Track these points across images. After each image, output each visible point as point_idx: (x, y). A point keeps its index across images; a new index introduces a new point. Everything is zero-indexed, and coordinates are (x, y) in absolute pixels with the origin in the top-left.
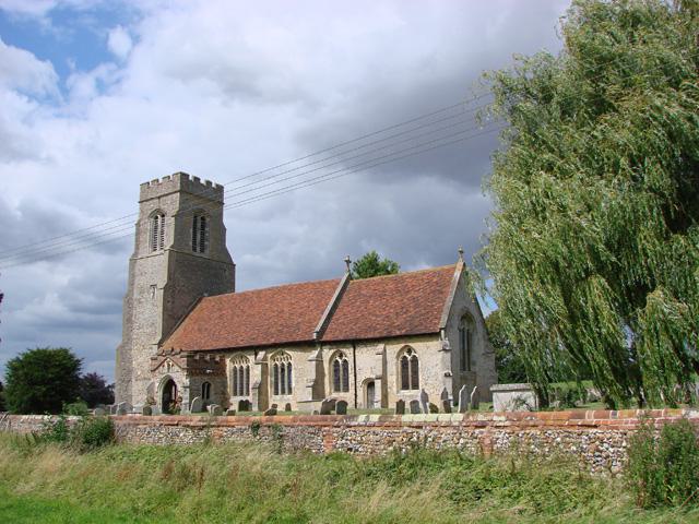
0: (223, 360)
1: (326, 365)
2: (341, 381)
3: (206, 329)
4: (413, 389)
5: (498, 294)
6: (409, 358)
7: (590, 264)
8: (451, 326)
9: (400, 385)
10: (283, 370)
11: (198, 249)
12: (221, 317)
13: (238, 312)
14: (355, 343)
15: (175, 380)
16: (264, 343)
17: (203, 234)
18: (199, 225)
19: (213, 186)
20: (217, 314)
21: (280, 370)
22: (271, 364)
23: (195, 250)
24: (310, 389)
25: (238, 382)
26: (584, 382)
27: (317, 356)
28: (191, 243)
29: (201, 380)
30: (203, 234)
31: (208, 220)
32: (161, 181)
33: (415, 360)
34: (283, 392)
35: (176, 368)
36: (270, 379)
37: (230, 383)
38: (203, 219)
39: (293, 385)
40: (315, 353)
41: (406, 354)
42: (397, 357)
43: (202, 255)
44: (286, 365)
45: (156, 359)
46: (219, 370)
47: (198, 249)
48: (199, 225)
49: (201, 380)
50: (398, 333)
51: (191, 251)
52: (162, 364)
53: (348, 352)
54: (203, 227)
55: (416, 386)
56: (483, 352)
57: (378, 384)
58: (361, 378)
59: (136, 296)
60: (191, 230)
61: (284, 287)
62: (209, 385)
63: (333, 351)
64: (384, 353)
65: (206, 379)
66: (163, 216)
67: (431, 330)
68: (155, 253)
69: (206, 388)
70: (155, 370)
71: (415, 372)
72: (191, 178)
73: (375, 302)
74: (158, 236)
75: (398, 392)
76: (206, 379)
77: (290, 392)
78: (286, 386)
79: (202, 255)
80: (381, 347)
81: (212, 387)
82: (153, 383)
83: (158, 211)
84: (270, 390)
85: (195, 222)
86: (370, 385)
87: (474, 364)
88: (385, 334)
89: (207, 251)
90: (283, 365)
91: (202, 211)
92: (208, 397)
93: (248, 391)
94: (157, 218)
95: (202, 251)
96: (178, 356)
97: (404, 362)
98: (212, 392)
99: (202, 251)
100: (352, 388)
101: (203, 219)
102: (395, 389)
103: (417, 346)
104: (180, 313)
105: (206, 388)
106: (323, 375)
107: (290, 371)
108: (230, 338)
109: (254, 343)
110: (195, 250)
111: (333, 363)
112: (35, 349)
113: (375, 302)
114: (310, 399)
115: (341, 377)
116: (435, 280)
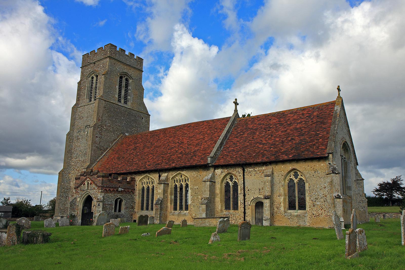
0: (133, 180)
1: (218, 186)
2: (231, 200)
3: (123, 158)
6: (296, 181)
9: (287, 206)
10: (181, 189)
11: (123, 101)
12: (135, 149)
13: (148, 144)
14: (244, 166)
15: (93, 196)
16: (166, 167)
17: (126, 91)
18: (124, 84)
20: (133, 147)
21: (178, 190)
22: (171, 184)
23: (119, 101)
24: (204, 206)
25: (145, 198)
26: (15, 227)
27: (211, 178)
28: (117, 96)
29: (112, 197)
30: (126, 91)
31: (130, 81)
32: (96, 52)
33: (302, 183)
34: (181, 208)
35: (94, 186)
36: (170, 197)
37: (137, 199)
39: (189, 202)
40: (207, 175)
41: (292, 177)
42: (285, 179)
43: (125, 105)
44: (184, 186)
45: (79, 179)
46: (130, 189)
48: (124, 84)
49: (112, 197)
50: (286, 158)
51: (116, 102)
52: (83, 183)
53: (237, 172)
54: (127, 86)
55: (187, 209)
57: (267, 203)
58: (250, 197)
59: (75, 134)
60: (117, 87)
61: (184, 126)
63: (224, 174)
64: (272, 175)
65: (119, 196)
66: (97, 76)
67: (319, 154)
68: (90, 103)
69: (118, 203)
70: (78, 187)
72: (118, 49)
73: (260, 133)
74: (93, 91)
75: (285, 212)
76: (119, 196)
77: (187, 209)
78: (184, 204)
79: (125, 105)
80: (268, 169)
81: (123, 203)
82: (76, 198)
83: (93, 72)
84: (170, 206)
85: (121, 82)
86: (259, 205)
88: (273, 158)
89: (129, 103)
90: (181, 185)
92: (120, 211)
93: (152, 206)
94: (93, 78)
95: (125, 103)
96: (96, 176)
97: (291, 185)
98: (123, 207)
99: (125, 103)
101: (127, 80)
102: (282, 209)
103: (299, 166)
104: (105, 147)
105: (118, 203)
107: (187, 191)
108: (140, 163)
109: (159, 167)
110: (119, 101)
111: (224, 185)
113: (260, 133)
114: (204, 216)
115: (231, 196)
116: (315, 114)
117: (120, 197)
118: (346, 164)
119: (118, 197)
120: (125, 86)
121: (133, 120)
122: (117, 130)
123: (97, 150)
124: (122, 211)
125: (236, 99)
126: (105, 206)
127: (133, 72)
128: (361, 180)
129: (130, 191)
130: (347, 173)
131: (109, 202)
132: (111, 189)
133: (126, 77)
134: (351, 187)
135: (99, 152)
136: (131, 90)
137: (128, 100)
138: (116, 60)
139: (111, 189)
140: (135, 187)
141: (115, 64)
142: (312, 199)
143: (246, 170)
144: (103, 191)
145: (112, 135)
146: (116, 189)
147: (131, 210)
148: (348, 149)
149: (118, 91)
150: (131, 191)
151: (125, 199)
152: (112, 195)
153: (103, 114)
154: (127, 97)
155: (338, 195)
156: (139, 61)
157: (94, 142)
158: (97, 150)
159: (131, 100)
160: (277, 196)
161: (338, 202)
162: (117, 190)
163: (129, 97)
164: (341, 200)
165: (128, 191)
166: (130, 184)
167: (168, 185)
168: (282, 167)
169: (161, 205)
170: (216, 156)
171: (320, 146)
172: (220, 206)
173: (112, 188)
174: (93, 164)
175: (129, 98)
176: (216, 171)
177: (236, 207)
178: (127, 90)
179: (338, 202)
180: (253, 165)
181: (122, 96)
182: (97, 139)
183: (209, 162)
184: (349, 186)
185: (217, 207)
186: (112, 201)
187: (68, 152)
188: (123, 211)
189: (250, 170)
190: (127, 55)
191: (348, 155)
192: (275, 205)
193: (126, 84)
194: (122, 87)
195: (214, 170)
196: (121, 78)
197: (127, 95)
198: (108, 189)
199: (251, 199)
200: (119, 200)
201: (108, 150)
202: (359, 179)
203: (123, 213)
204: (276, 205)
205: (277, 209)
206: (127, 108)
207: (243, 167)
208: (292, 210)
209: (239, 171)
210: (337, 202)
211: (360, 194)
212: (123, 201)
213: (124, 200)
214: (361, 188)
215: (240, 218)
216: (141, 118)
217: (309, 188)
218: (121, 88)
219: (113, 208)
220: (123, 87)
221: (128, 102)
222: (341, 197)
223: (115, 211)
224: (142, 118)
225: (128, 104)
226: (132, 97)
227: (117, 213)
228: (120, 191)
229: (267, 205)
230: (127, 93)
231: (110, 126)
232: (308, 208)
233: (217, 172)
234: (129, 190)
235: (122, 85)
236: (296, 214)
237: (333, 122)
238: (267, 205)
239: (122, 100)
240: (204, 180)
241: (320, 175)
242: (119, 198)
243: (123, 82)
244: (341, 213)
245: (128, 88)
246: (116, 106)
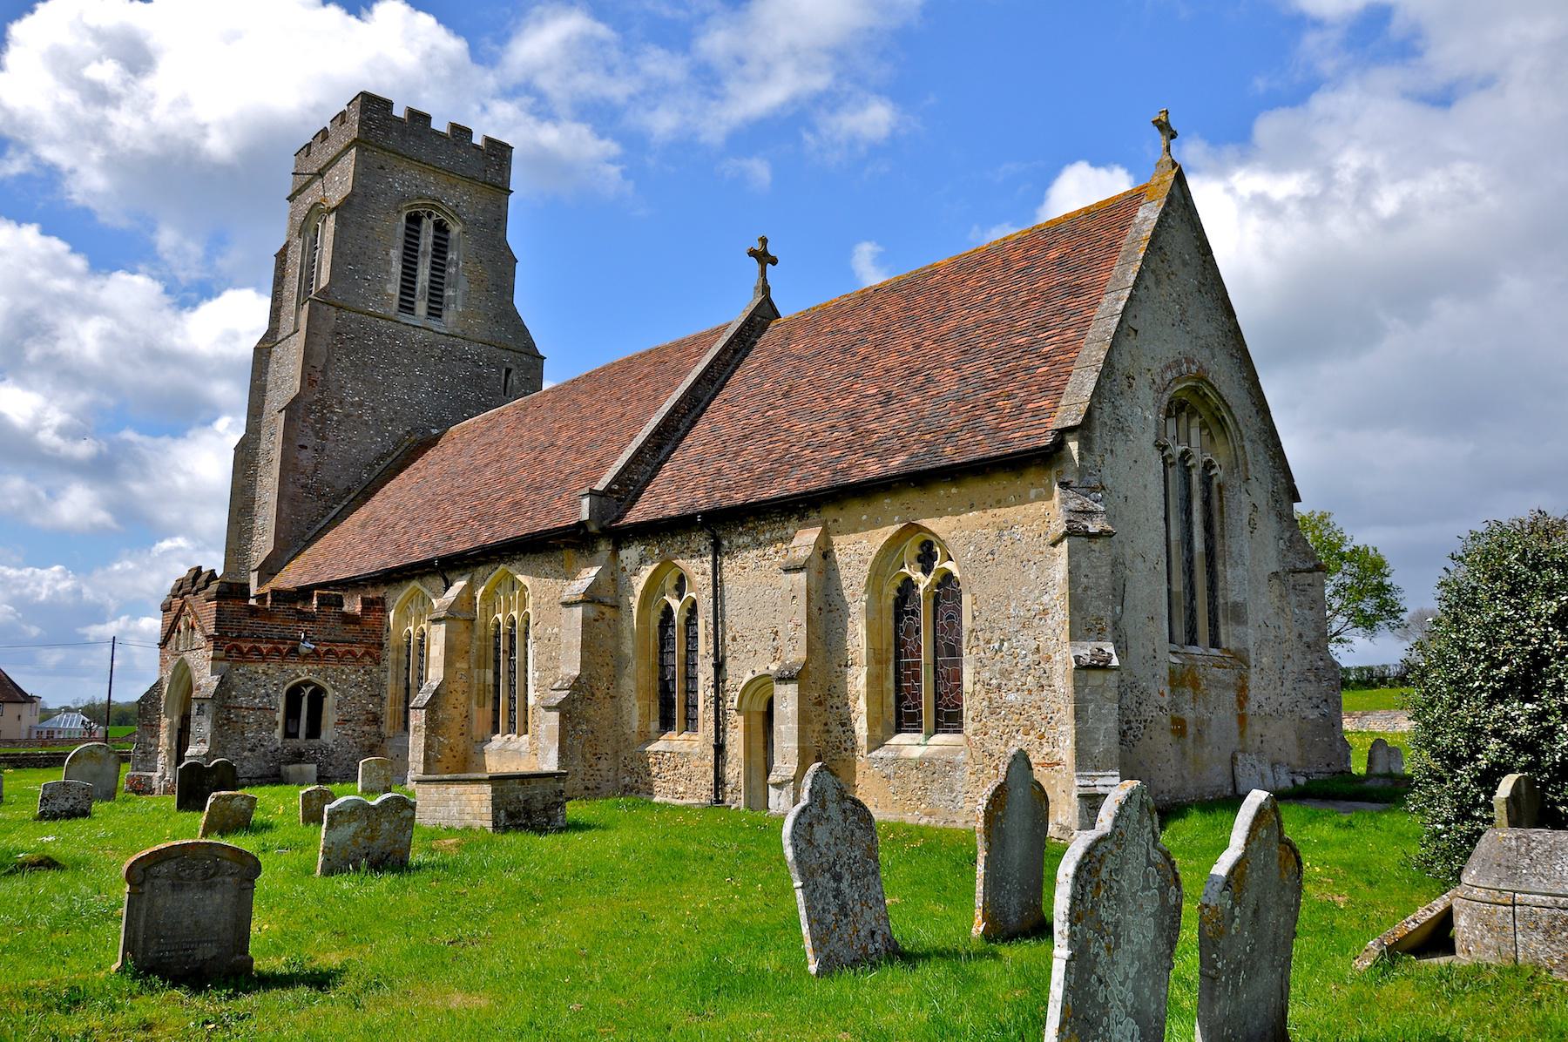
4: (938, 728)
5: (1119, 447)
7: (452, 841)
8: (1120, 427)
11: (421, 307)
17: (438, 268)
19: (477, 140)
23: (407, 306)
28: (394, 289)
30: (438, 268)
31: (455, 229)
38: (440, 227)
43: (433, 324)
47: (421, 307)
50: (874, 469)
54: (440, 249)
56: (1275, 567)
58: (740, 674)
60: (396, 254)
62: (318, 696)
65: (304, 672)
67: (1020, 439)
71: (949, 650)
80: (805, 539)
81: (330, 702)
87: (1238, 614)
89: (450, 316)
91: (435, 204)
92: (314, 730)
95: (435, 312)
98: (330, 716)
99: (435, 312)
100: (705, 713)
101: (440, 227)
106: (618, 665)
110: (407, 306)
112: (1481, 528)
117: (313, 678)
118: (1220, 492)
119: (300, 679)
120: (434, 250)
121: (464, 380)
122: (391, 420)
123: (307, 497)
124: (323, 736)
125: (764, 241)
126: (237, 716)
127: (466, 195)
128: (1309, 571)
129: (359, 651)
130: (1223, 537)
131: (255, 698)
132: (264, 647)
133: (437, 216)
134: (1244, 605)
135: (314, 504)
136: (457, 264)
137: (445, 302)
138: (389, 152)
139: (264, 647)
140: (384, 638)
141: (382, 168)
142: (986, 675)
143: (725, 543)
144: (222, 654)
145: (371, 439)
146: (286, 643)
147: (366, 728)
148: (1223, 417)
149: (397, 268)
150: (367, 653)
151: (334, 688)
152: (270, 672)
153: (328, 360)
154: (442, 290)
155: (1099, 650)
156: (494, 156)
157: (290, 467)
158: (307, 497)
159: (459, 302)
160: (840, 666)
161: (1091, 692)
162: (294, 650)
163: (449, 292)
164: (1113, 678)
165: (349, 652)
166: (359, 624)
167: (470, 627)
168: (864, 517)
169: (434, 712)
170: (627, 486)
171: (1033, 397)
172: (636, 712)
173: (269, 640)
174: (289, 550)
175: (451, 293)
176: (623, 554)
177: (690, 723)
178: (444, 266)
179: (1091, 692)
180: (752, 518)
181: (418, 290)
182: (304, 454)
183: (585, 516)
184: (1236, 605)
185: (626, 718)
186: (268, 695)
187: (240, 511)
188: (329, 734)
189: (741, 541)
190: (476, 147)
191: (1232, 449)
192: (835, 710)
193: (435, 243)
194: (419, 254)
195: (615, 553)
196: (414, 220)
197: (442, 284)
198: (245, 646)
199: (745, 681)
200: (307, 691)
201: (352, 496)
202: (1300, 566)
203: (329, 741)
204: (837, 708)
205: (841, 729)
206: (438, 333)
207: (710, 529)
208: (911, 732)
209: (702, 549)
210: (1087, 691)
211: (1305, 639)
212: (326, 692)
213: (330, 691)
214: (1311, 609)
215: (703, 769)
216: (504, 370)
217: (974, 618)
218: (416, 257)
219: (277, 723)
220: (425, 253)
221: (445, 313)
222: (1115, 662)
223: (289, 734)
224: (508, 371)
225: (444, 318)
226: (459, 293)
227: (301, 741)
228: (307, 655)
229: (789, 709)
230: (443, 278)
231: (361, 405)
232: (969, 726)
233: (625, 560)
234: (356, 650)
235: (417, 245)
236: (917, 752)
237: (1115, 277)
238: (789, 709)
239: (417, 303)
240: (565, 598)
241: (1020, 549)
242: (307, 683)
243: (423, 234)
244: (1107, 750)
245: (445, 259)
246: (390, 328)
